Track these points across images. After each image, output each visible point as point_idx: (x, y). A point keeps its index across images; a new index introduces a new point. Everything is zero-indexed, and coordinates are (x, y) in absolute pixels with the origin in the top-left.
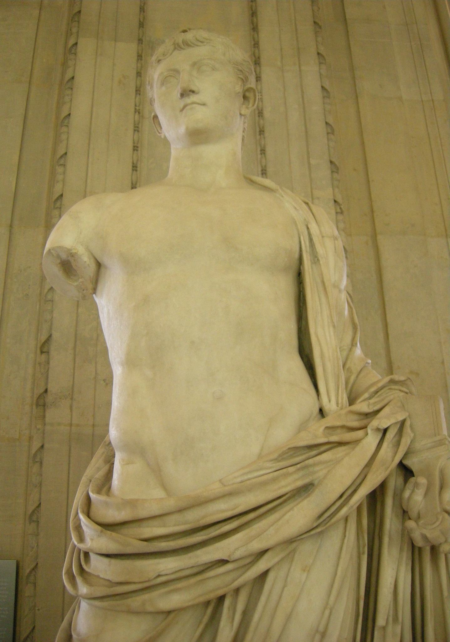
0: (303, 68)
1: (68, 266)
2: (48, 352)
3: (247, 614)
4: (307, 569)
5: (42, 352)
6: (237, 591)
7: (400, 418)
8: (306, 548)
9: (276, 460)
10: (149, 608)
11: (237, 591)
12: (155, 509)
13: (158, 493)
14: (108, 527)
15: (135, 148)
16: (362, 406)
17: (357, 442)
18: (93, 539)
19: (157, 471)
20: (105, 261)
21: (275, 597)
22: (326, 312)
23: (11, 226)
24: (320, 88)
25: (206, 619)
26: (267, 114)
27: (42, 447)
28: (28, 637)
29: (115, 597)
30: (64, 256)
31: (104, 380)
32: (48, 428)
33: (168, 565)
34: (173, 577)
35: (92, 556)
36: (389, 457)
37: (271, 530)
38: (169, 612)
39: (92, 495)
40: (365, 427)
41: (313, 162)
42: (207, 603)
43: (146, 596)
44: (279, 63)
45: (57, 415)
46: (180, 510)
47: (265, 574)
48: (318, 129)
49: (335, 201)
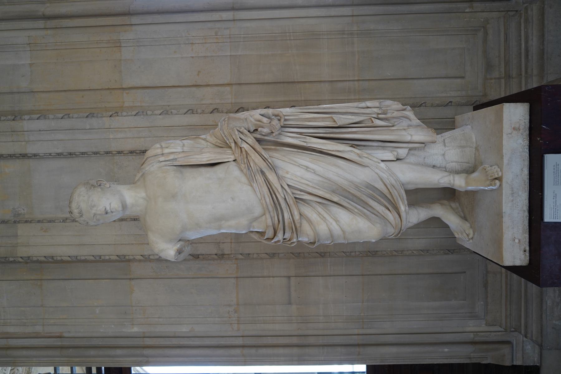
0: (26, 130)
1: (179, 252)
2: (198, 255)
4: (287, 173)
5: (198, 258)
6: (293, 193)
7: (237, 133)
8: (280, 173)
11: (293, 193)
16: (233, 145)
17: (246, 151)
19: (256, 219)
20: (179, 238)
21: (296, 182)
22: (197, 156)
24: (38, 120)
25: (303, 203)
26: (59, 151)
27: (241, 254)
29: (296, 230)
32: (233, 252)
33: (286, 215)
36: (251, 139)
37: (276, 185)
41: (88, 127)
43: (296, 222)
44: (23, 143)
47: (288, 185)
48: (66, 123)
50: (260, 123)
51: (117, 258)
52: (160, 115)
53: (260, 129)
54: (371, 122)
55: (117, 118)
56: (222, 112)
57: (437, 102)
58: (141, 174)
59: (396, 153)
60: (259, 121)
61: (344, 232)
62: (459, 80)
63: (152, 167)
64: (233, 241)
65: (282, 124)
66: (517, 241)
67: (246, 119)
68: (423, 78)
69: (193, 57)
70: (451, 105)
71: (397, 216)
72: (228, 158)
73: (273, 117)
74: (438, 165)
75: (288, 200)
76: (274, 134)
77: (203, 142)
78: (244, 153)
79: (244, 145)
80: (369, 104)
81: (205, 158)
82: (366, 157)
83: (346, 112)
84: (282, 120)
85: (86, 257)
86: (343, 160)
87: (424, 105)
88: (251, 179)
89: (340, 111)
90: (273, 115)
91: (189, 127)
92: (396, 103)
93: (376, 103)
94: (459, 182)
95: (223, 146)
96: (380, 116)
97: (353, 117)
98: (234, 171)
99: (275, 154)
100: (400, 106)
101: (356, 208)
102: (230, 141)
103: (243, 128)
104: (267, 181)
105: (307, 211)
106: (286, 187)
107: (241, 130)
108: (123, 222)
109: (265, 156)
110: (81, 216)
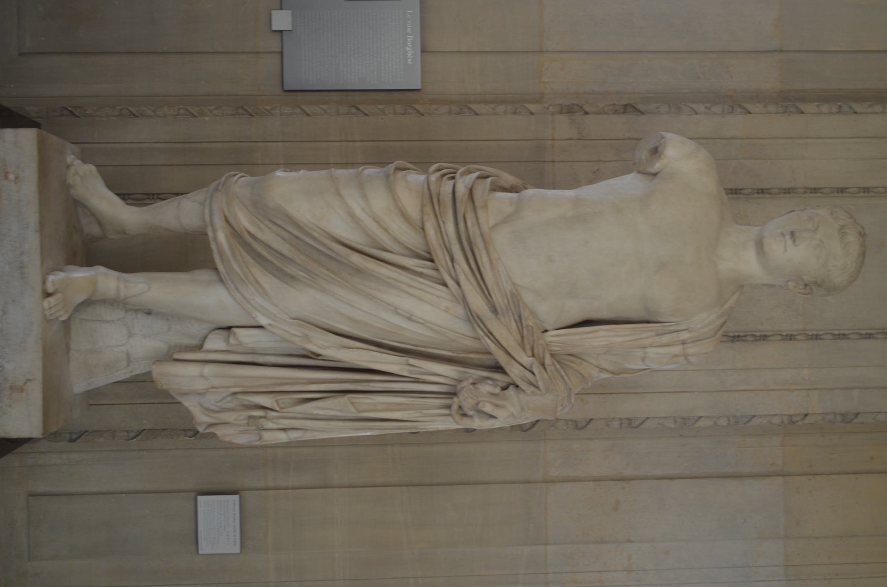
1: (656, 152)
2: (625, 112)
3: (420, 275)
4: (447, 310)
6: (437, 270)
7: (540, 384)
8: (460, 310)
9: (512, 293)
10: (425, 217)
11: (437, 270)
12: (482, 219)
13: (492, 222)
14: (471, 192)
15: (867, 190)
16: (548, 360)
17: (524, 349)
18: (463, 184)
19: (507, 220)
23: (781, 51)
24: (590, 417)
27: (532, 113)
28: (359, 110)
29: (431, 199)
30: (660, 149)
31: (598, 170)
33: (450, 228)
34: (443, 230)
35: (452, 182)
36: (515, 371)
38: (423, 229)
39: (489, 179)
40: (533, 356)
42: (430, 253)
43: (432, 215)
45: (563, 126)
46: (482, 235)
47: (445, 285)
49: (806, 415)
50: (497, 402)
51: (802, 106)
52: (701, 417)
53: (497, 390)
54: (280, 402)
55: (792, 412)
56: (566, 421)
57: (102, 440)
58: (727, 306)
59: (232, 341)
60: (497, 406)
61: (339, 195)
62: (41, 488)
63: (704, 320)
64: (550, 142)
65: (456, 399)
66: (12, 177)
67: (523, 409)
68: (122, 493)
69: (629, 541)
70: (71, 433)
71: (231, 220)
72: (558, 336)
73: (471, 413)
74: (140, 315)
75: (448, 258)
76: (471, 381)
77: (605, 365)
78: (527, 346)
79: (526, 360)
80: (282, 437)
81: (600, 336)
82: (295, 335)
83: (329, 421)
84: (455, 407)
85: (870, 110)
86: (340, 332)
87: (132, 435)
88: (515, 299)
89: (341, 424)
90: (471, 417)
91: (640, 390)
92: (227, 439)
93: (269, 437)
94: (107, 281)
95: (567, 357)
96: (260, 413)
97: (316, 412)
98: (547, 310)
99: (470, 343)
100: (219, 432)
101: (315, 239)
102: (553, 368)
103: (528, 392)
104: (487, 294)
105: (411, 238)
106: (450, 282)
107: (533, 389)
108: (787, 185)
109: (488, 341)
110: (842, 227)
